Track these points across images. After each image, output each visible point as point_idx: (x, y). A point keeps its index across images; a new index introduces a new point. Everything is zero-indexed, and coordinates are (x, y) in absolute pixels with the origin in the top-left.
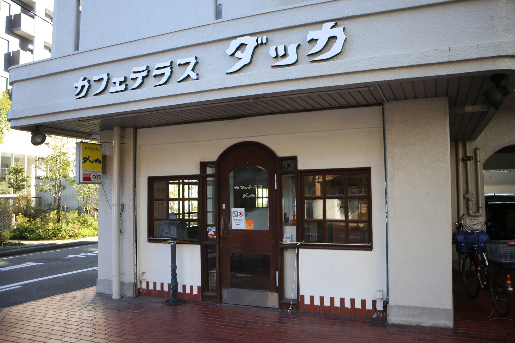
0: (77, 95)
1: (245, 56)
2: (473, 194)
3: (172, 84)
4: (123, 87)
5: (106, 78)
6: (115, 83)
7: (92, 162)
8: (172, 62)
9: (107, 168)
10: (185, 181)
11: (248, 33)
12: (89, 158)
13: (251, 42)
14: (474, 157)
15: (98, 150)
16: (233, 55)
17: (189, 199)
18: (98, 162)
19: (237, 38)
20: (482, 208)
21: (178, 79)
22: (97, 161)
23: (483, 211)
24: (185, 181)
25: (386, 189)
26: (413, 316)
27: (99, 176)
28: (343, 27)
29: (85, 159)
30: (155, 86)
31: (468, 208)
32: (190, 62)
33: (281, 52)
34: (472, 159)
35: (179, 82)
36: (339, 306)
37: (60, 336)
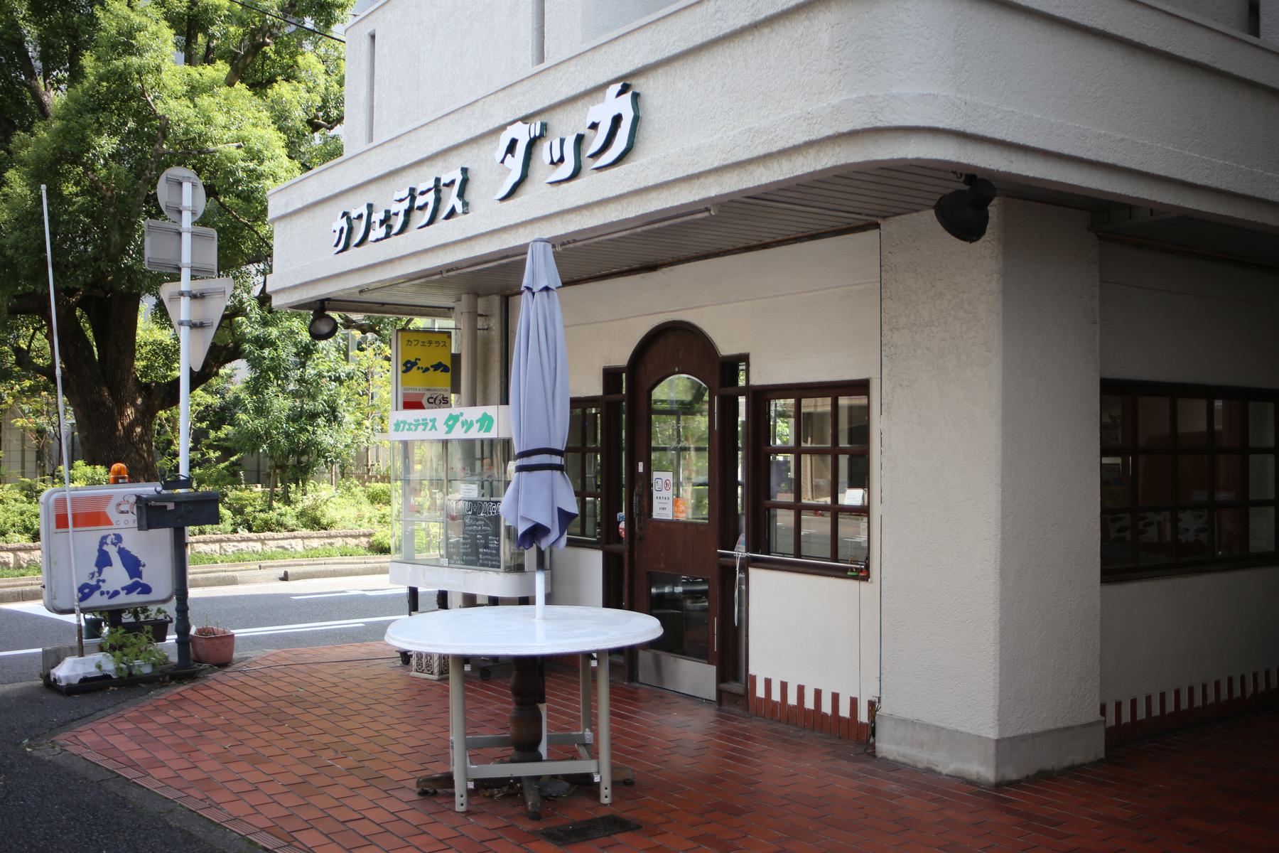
0: (337, 245)
7: (427, 370)
12: (101, 584)
13: (522, 134)
16: (502, 162)
18: (140, 589)
19: (509, 128)
21: (495, 194)
22: (437, 367)
26: (921, 745)
27: (443, 398)
29: (87, 591)
35: (503, 199)
36: (813, 708)
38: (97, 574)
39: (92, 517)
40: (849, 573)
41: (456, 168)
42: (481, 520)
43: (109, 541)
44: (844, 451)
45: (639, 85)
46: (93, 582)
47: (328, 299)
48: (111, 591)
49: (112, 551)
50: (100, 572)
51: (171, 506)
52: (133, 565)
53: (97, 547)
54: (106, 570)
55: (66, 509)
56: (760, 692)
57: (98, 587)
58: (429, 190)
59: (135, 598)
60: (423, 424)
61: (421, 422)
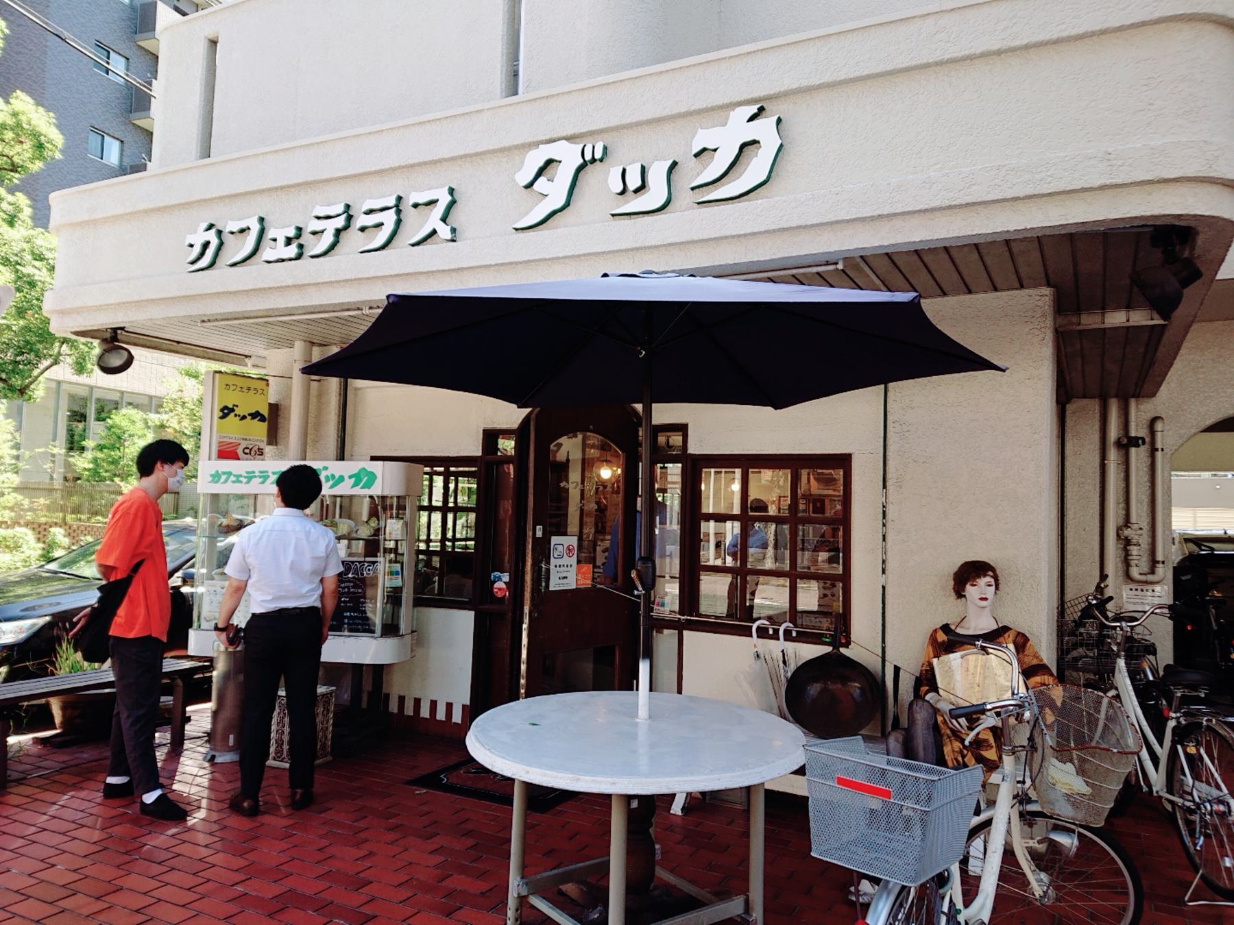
0: (193, 263)
1: (555, 190)
2: (1141, 529)
4: (292, 250)
5: (255, 228)
6: (275, 240)
7: (244, 418)
8: (399, 199)
9: (281, 433)
10: (452, 469)
13: (569, 157)
14: (1147, 440)
15: (260, 392)
16: (530, 186)
20: (1163, 562)
21: (410, 239)
23: (1165, 573)
24: (452, 469)
25: (884, 507)
27: (259, 449)
28: (777, 117)
29: (226, 411)
30: (362, 252)
31: (1127, 563)
32: (437, 201)
33: (634, 181)
34: (1144, 443)
35: (413, 245)
40: (824, 639)
41: (442, 186)
42: (349, 581)
47: (122, 329)
56: (394, 707)
60: (260, 477)
61: (257, 474)
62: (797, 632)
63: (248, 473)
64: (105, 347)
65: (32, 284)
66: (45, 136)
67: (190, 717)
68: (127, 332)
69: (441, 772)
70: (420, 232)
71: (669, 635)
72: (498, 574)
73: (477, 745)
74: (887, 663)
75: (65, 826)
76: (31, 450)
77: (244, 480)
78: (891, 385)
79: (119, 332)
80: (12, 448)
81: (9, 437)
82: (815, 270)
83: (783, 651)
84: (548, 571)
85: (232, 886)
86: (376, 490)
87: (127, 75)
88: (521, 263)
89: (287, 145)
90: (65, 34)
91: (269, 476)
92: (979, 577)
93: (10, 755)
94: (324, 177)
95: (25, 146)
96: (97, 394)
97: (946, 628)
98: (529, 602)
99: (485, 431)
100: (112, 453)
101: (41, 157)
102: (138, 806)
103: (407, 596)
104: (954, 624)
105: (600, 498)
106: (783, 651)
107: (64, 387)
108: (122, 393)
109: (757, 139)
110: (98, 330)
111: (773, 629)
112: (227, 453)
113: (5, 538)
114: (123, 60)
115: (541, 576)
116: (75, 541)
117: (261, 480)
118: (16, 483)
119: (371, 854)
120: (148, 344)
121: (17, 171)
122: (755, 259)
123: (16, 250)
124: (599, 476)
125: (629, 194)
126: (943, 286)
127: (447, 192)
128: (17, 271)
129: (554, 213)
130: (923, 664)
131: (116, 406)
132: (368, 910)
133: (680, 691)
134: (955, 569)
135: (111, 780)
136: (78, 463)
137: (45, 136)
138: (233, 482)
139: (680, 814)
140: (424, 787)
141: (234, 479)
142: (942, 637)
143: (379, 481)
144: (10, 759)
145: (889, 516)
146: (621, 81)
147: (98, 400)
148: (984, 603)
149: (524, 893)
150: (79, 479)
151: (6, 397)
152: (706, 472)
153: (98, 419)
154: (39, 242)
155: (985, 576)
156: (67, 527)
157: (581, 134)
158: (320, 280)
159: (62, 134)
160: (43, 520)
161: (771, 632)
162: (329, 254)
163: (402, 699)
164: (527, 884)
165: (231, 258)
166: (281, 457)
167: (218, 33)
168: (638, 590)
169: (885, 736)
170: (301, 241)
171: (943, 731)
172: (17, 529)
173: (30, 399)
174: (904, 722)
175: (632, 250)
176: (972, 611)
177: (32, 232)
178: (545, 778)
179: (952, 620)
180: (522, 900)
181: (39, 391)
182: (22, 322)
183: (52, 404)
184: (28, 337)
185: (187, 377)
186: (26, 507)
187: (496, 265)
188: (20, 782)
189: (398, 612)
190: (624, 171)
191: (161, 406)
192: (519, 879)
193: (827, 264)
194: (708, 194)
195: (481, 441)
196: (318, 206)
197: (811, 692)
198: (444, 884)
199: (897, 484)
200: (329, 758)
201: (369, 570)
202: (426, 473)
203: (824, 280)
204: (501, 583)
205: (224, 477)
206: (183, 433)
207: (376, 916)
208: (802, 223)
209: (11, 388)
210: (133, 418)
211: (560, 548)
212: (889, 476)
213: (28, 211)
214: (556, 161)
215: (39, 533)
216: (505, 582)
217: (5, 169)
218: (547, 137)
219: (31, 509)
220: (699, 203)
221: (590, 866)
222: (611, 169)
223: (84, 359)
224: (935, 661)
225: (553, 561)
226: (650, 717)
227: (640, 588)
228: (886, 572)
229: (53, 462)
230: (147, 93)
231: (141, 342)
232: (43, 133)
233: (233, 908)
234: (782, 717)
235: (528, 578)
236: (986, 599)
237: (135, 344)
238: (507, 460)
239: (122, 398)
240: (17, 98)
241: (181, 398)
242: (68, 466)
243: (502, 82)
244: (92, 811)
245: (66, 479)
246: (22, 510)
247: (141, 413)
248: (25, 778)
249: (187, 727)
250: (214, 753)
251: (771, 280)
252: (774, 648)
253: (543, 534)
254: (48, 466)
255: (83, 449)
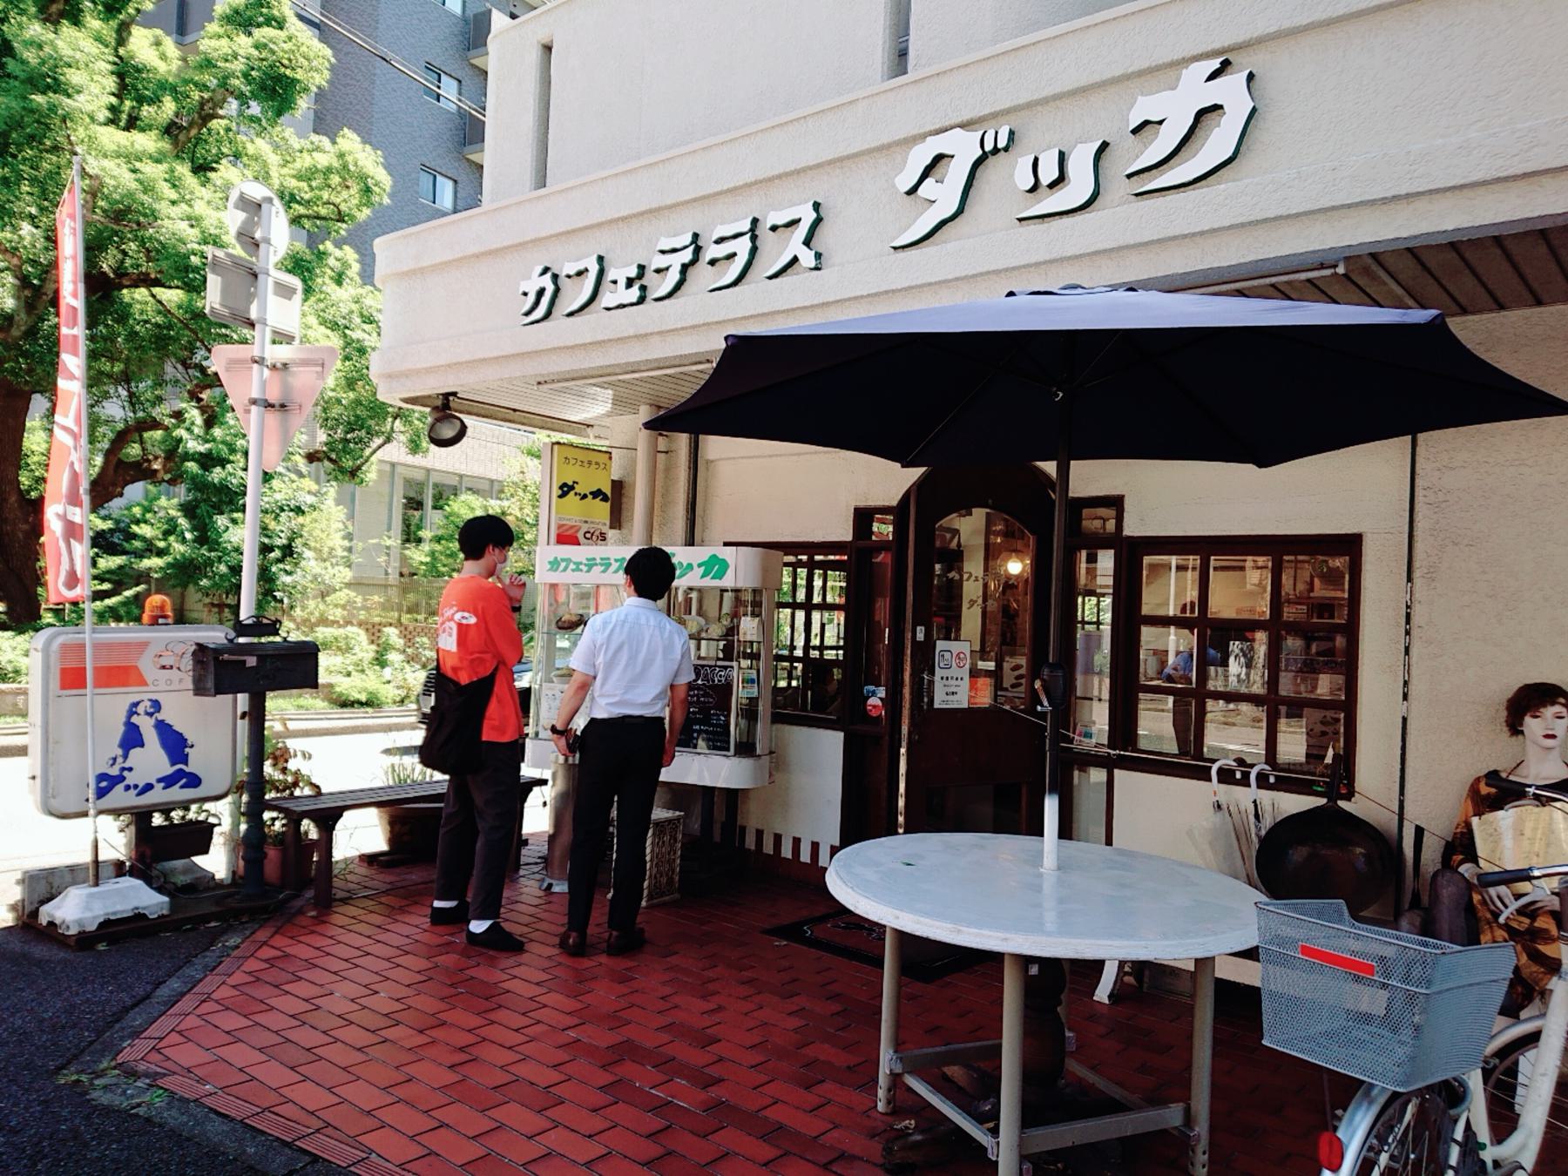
0: (527, 314)
1: (944, 194)
3: (1246, 181)
4: (634, 293)
5: (594, 269)
6: (615, 282)
7: (585, 496)
8: (755, 221)
10: (818, 558)
11: (958, 120)
12: (126, 773)
13: (964, 148)
15: (602, 466)
16: (913, 191)
17: (824, 606)
18: (184, 780)
22: (597, 494)
24: (818, 558)
25: (1408, 607)
27: (601, 533)
28: (1247, 72)
29: (565, 489)
32: (800, 220)
33: (1048, 173)
35: (770, 278)
37: (538, 927)
38: (120, 760)
39: (118, 675)
43: (141, 709)
44: (1079, 622)
45: (1272, 64)
46: (115, 771)
47: (454, 394)
48: (141, 785)
49: (146, 725)
50: (125, 757)
51: (252, 661)
52: (175, 744)
53: (123, 719)
54: (135, 753)
55: (1177, 579)
56: (750, 843)
57: (121, 778)
58: (686, 247)
59: (177, 793)
60: (602, 565)
61: (598, 561)
62: (1276, 776)
63: (588, 560)
64: (437, 415)
65: (362, 351)
66: (372, 178)
67: (527, 840)
68: (459, 398)
69: (806, 923)
70: (782, 257)
71: (1098, 775)
72: (872, 688)
73: (839, 882)
74: (1406, 822)
75: (390, 952)
76: (364, 542)
77: (585, 569)
78: (1421, 437)
79: (451, 398)
80: (344, 538)
81: (341, 526)
82: (1303, 276)
83: (1255, 802)
84: (931, 683)
85: (563, 1030)
86: (728, 581)
87: (460, 100)
88: (900, 290)
89: (629, 166)
90: (390, 55)
91: (610, 564)
92: (1545, 706)
93: (336, 872)
94: (669, 202)
95: (351, 192)
96: (434, 478)
97: (1493, 776)
98: (907, 721)
99: (855, 509)
100: (451, 545)
101: (369, 204)
102: (464, 935)
103: (764, 708)
104: (1505, 771)
105: (1009, 601)
106: (1255, 802)
107: (399, 469)
108: (461, 476)
109: (1219, 103)
110: (429, 397)
111: (1242, 772)
112: (566, 538)
113: (336, 639)
114: (455, 83)
115: (922, 690)
116: (410, 644)
117: (603, 568)
118: (348, 578)
119: (720, 1009)
120: (483, 412)
121: (344, 221)
122: (1215, 265)
123: (345, 311)
124: (1006, 570)
125: (1043, 190)
126: (1499, 294)
127: (811, 208)
128: (345, 336)
129: (943, 223)
130: (1458, 825)
131: (455, 492)
132: (714, 1071)
133: (1109, 842)
134: (1510, 694)
135: (437, 904)
136: (414, 556)
137: (372, 178)
138: (573, 570)
139: (1107, 1002)
140: (786, 939)
141: (574, 567)
142: (1485, 790)
143: (730, 573)
144: (336, 876)
145: (1415, 620)
146: (1034, 44)
147: (436, 485)
148: (1550, 742)
149: (898, 1070)
150: (415, 574)
151: (336, 479)
152: (1152, 567)
153: (435, 507)
154: (368, 301)
155: (1553, 703)
156: (403, 629)
157: (980, 118)
158: (664, 328)
159: (390, 175)
160: (377, 620)
161: (1238, 775)
162: (675, 295)
163: (760, 833)
164: (901, 1059)
165: (568, 307)
166: (625, 542)
167: (552, 41)
168: (1042, 705)
169: (1397, 915)
170: (644, 282)
171: (1480, 914)
172: (349, 628)
173: (362, 482)
174: (1425, 900)
175: (1045, 262)
176: (1532, 753)
177: (360, 291)
178: (918, 926)
179: (1501, 764)
180: (895, 1079)
181: (371, 474)
182: (352, 395)
183: (386, 490)
184: (358, 412)
185: (529, 457)
186: (359, 605)
187: (869, 295)
188: (345, 901)
189: (755, 729)
190: (1036, 160)
191: (502, 491)
192: (891, 1052)
193: (1322, 267)
194: (1150, 181)
195: (852, 523)
196: (662, 238)
197: (1295, 858)
198: (803, 1051)
199: (1429, 576)
200: (677, 896)
201: (721, 676)
202: (787, 564)
203: (1319, 291)
204: (876, 699)
205: (563, 565)
206: (526, 522)
207: (723, 1080)
208: (1283, 212)
209: (342, 470)
210: (473, 506)
211: (947, 655)
212: (1417, 564)
213: (356, 267)
214: (948, 156)
215: (373, 634)
216: (880, 698)
217: (332, 219)
218: (937, 126)
219: (365, 608)
220: (1137, 195)
221: (981, 1047)
222: (1019, 160)
223: (419, 437)
224: (1475, 821)
225: (939, 673)
226: (1059, 868)
227: (1046, 703)
228: (1410, 697)
229: (388, 555)
230: (478, 119)
231: (475, 411)
232: (371, 174)
233: (563, 1056)
234: (1250, 885)
235: (907, 691)
236: (1553, 737)
237: (469, 413)
238: (883, 546)
239: (461, 483)
240: (343, 136)
241: (522, 481)
242: (404, 560)
243: (883, 63)
244: (417, 937)
245: (401, 575)
246: (355, 608)
247: (481, 499)
248: (350, 898)
249: (524, 851)
250: (551, 881)
251: (1240, 293)
252: (1243, 797)
253: (925, 635)
254: (382, 559)
255: (419, 541)
